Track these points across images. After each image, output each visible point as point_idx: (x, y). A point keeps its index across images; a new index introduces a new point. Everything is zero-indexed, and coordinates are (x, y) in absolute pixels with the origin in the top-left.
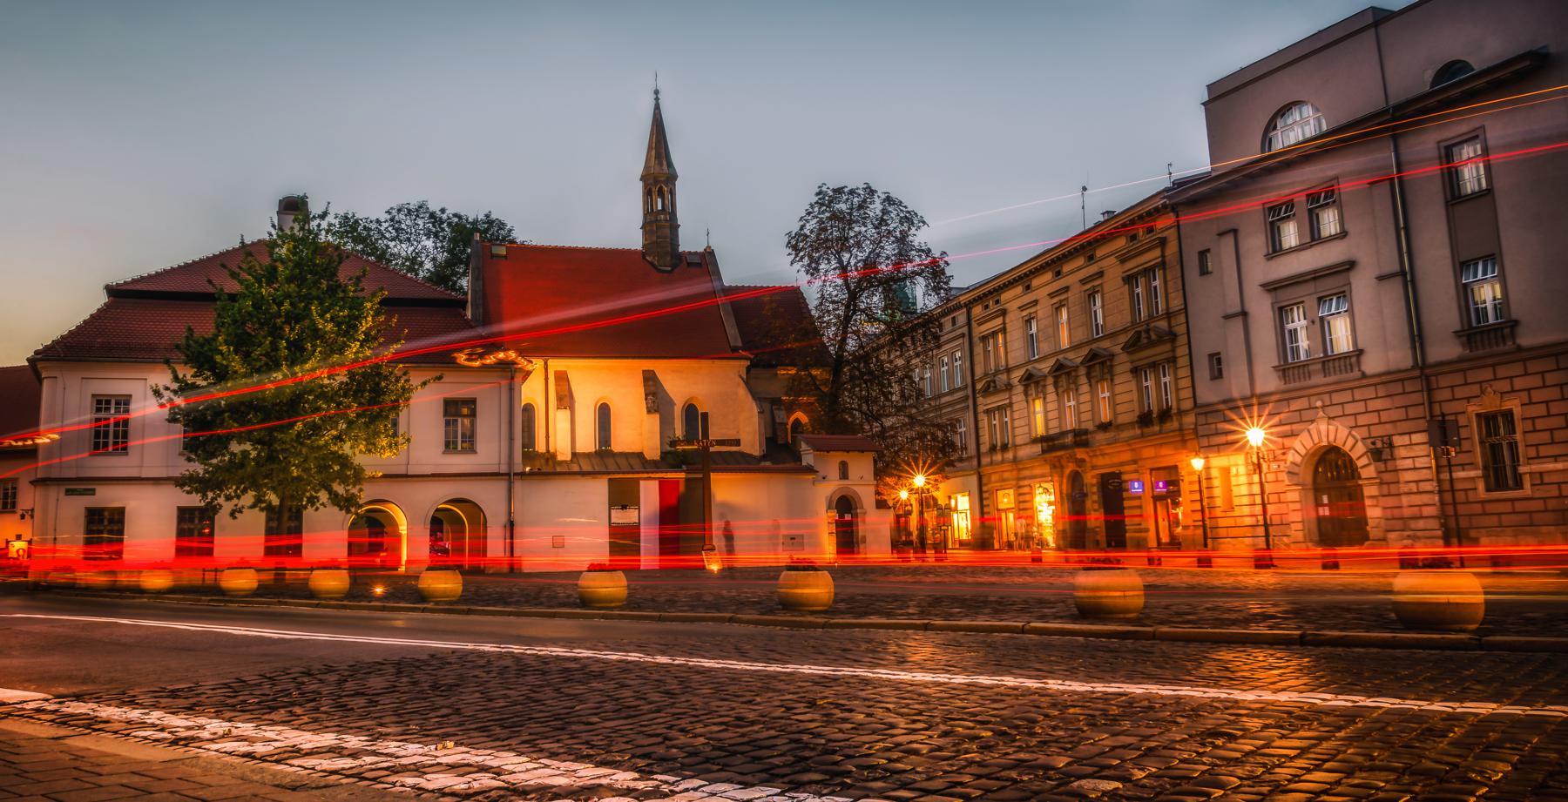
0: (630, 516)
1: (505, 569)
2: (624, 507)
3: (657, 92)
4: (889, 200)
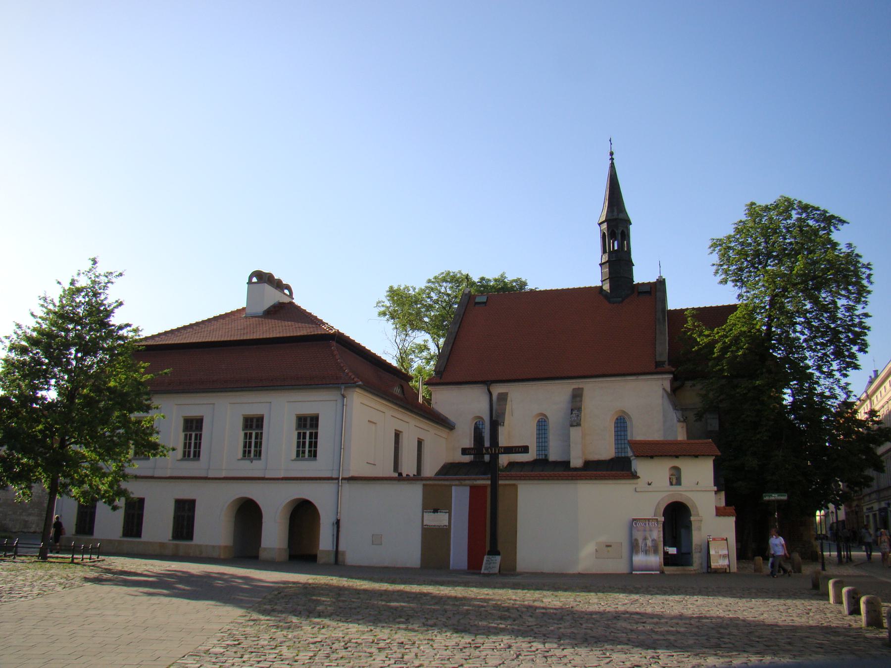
0: (440, 519)
1: (332, 559)
2: (436, 511)
3: (612, 154)
4: (805, 208)
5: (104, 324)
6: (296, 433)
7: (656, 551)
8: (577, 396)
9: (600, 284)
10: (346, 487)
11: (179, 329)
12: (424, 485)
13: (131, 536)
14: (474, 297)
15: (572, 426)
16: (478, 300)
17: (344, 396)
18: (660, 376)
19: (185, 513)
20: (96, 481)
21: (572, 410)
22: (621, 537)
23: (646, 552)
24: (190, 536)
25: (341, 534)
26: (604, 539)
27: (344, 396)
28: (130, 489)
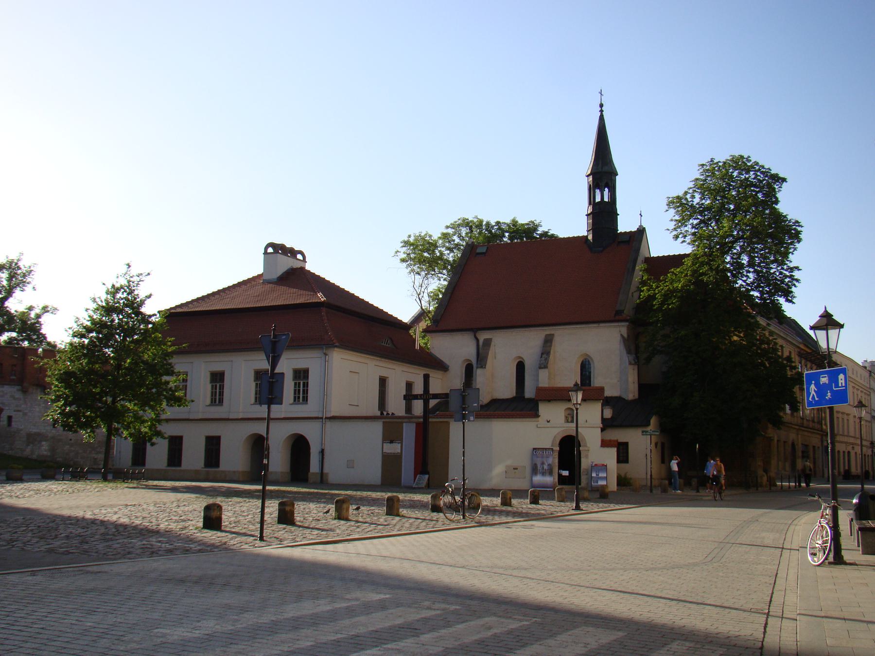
1: (319, 479)
2: (391, 442)
3: (601, 106)
5: (138, 313)
6: (293, 384)
7: (551, 473)
8: (548, 341)
9: (585, 234)
10: (329, 424)
11: (208, 296)
12: (384, 422)
13: (174, 465)
14: (477, 247)
15: (540, 368)
16: (479, 250)
17: (326, 354)
18: (616, 324)
19: (213, 446)
20: (137, 425)
21: (542, 354)
22: (525, 461)
23: (543, 474)
24: (217, 465)
25: (326, 460)
26: (509, 462)
27: (326, 354)
28: (163, 431)
